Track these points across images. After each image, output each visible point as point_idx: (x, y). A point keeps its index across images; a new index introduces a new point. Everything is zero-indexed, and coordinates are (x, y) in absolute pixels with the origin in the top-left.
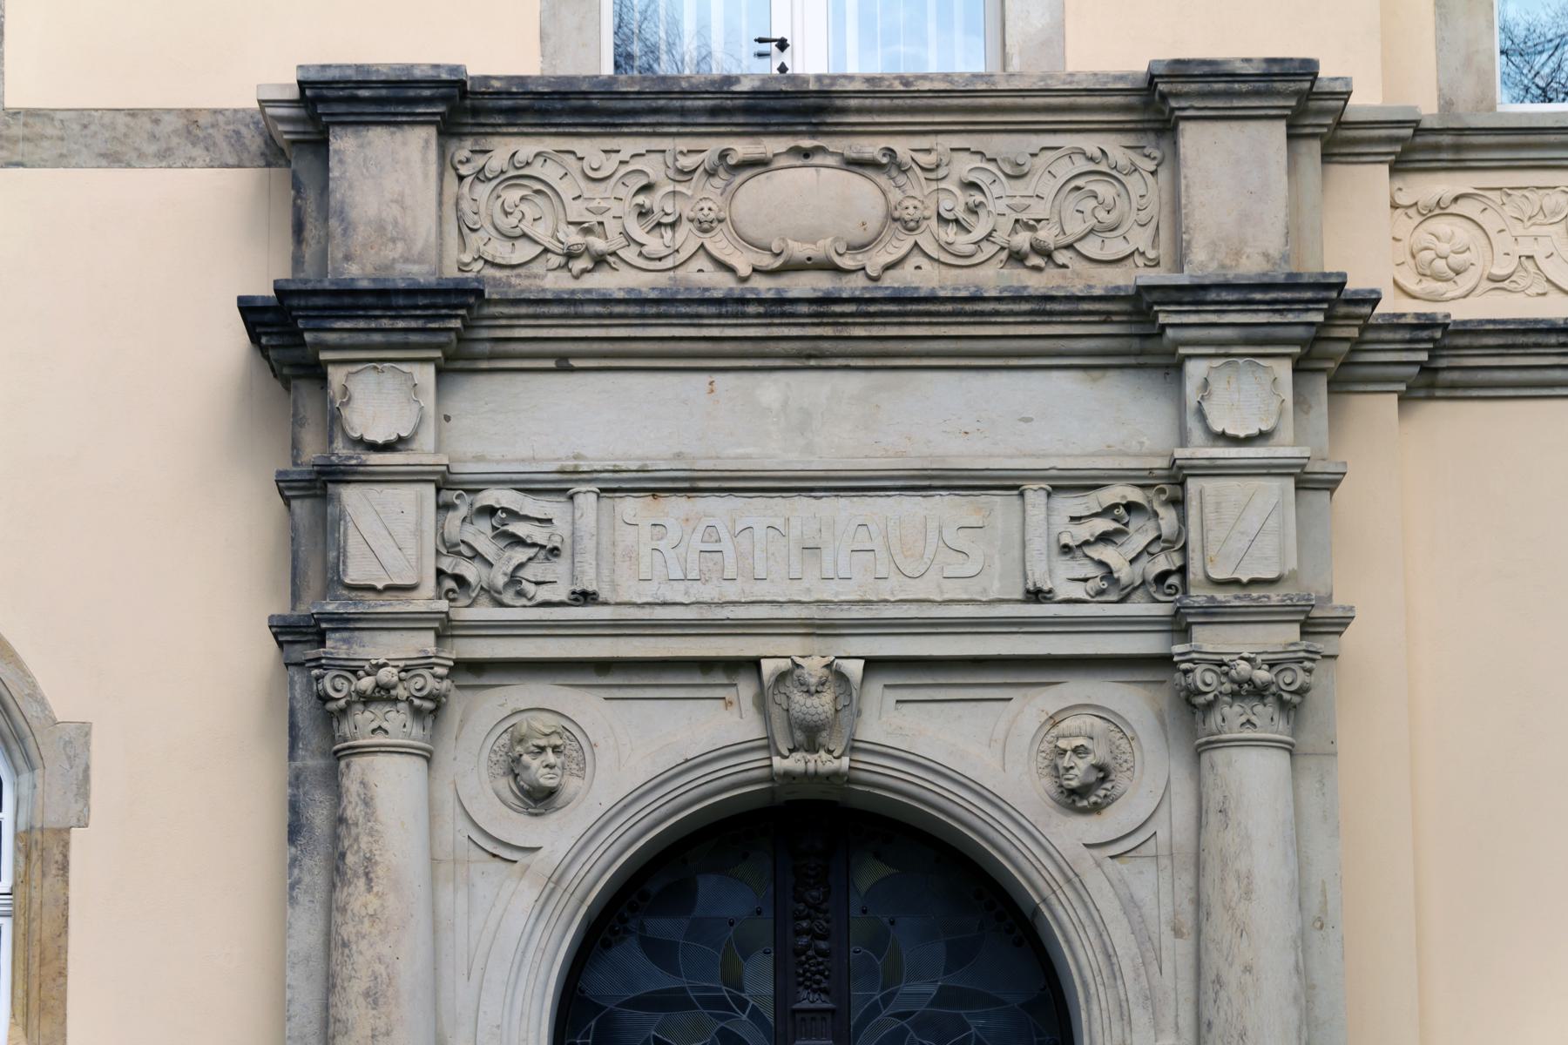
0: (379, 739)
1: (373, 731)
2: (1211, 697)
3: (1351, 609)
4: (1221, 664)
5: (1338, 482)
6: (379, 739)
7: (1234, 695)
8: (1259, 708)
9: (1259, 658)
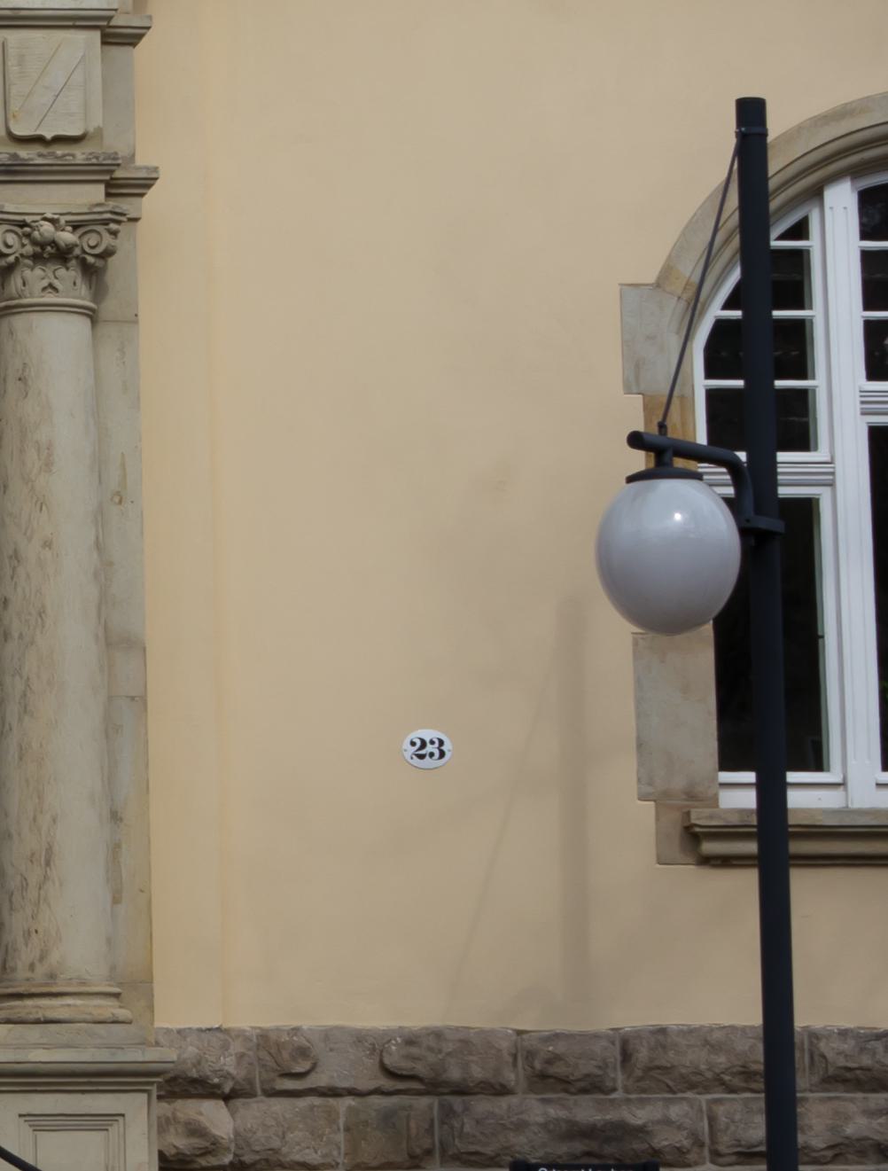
0: (50, 298)
1: (44, 289)
2: (11, 259)
3: (156, 169)
4: (23, 224)
5: (140, 37)
6: (50, 298)
7: (37, 258)
8: (62, 272)
9: (63, 220)
